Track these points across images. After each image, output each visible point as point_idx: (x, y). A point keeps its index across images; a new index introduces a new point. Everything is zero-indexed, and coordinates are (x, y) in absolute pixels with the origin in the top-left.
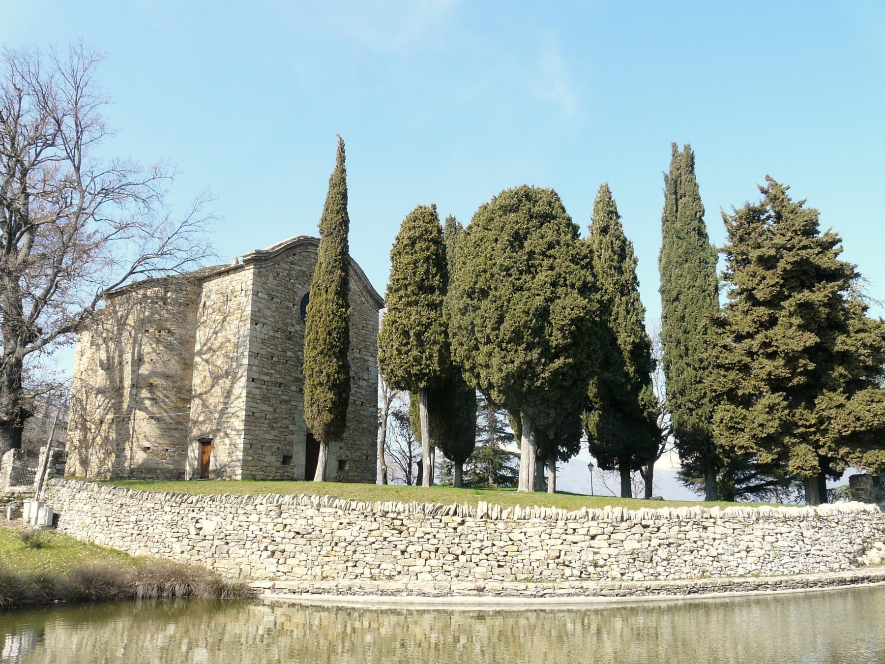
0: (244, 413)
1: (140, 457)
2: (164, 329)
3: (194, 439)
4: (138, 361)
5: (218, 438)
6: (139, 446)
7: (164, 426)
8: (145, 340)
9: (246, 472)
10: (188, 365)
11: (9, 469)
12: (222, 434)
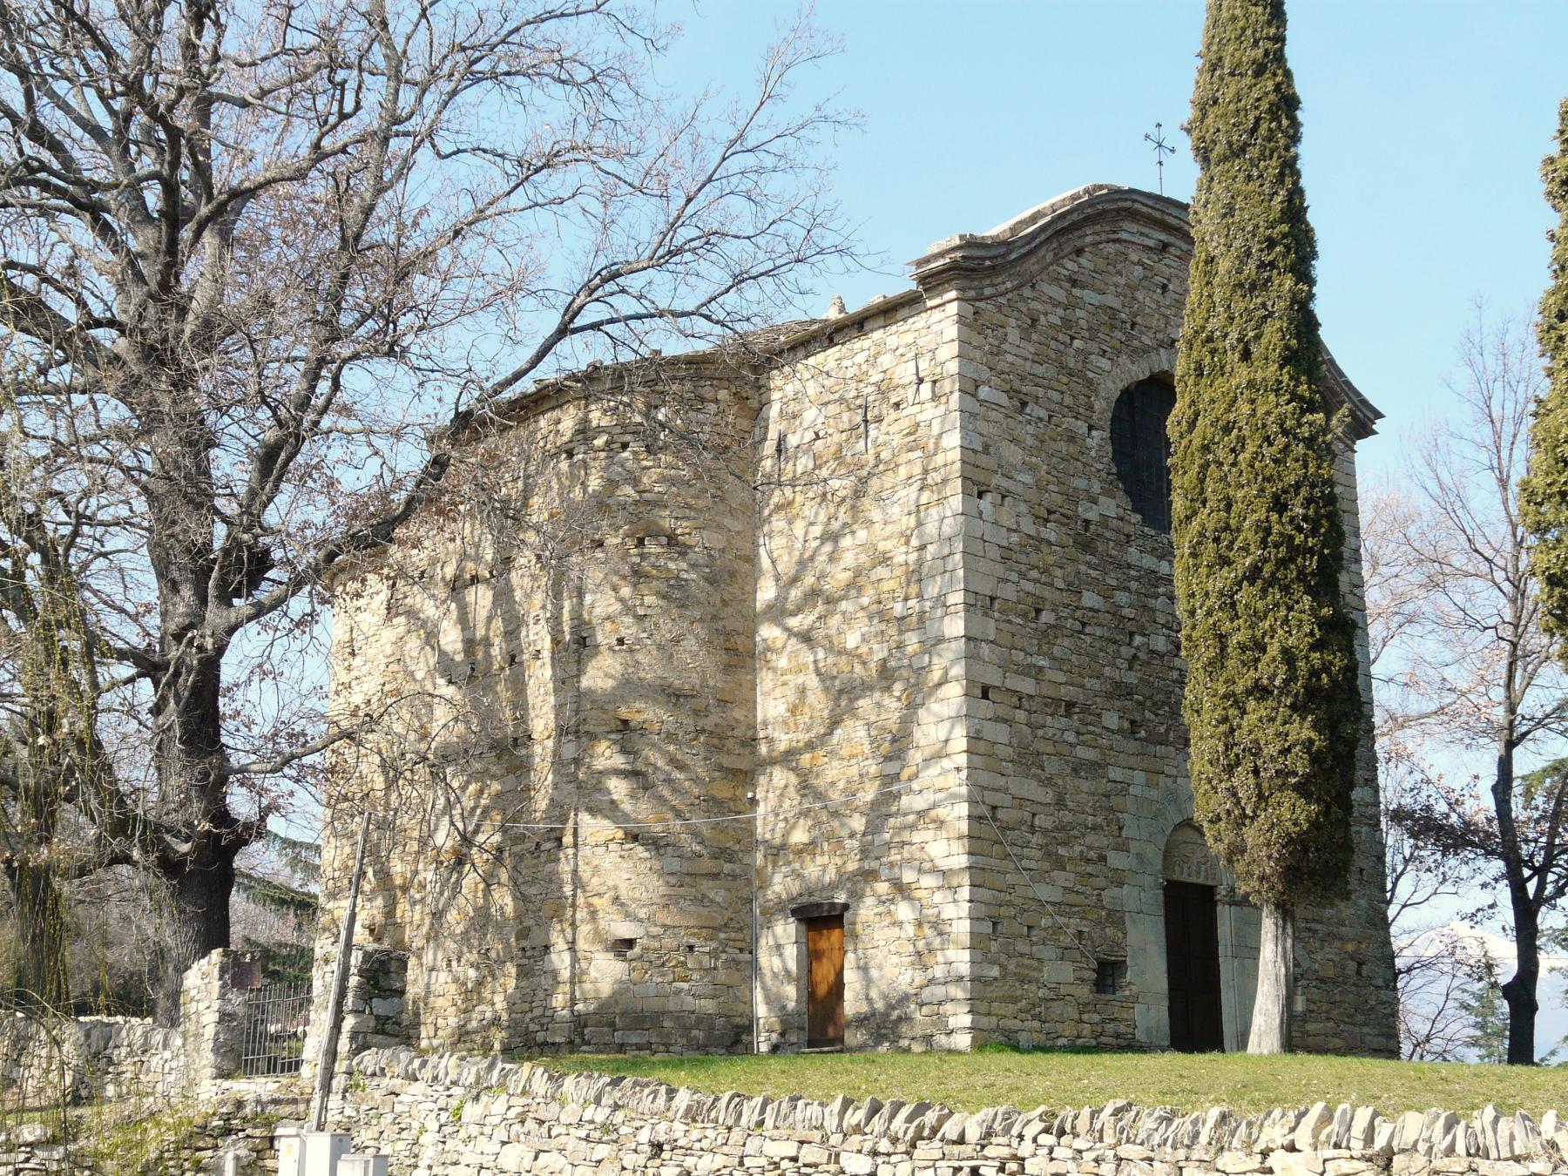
0: (963, 809)
1: (605, 973)
2: (655, 535)
3: (780, 908)
4: (577, 646)
5: (870, 901)
6: (598, 936)
7: (675, 865)
8: (595, 575)
9: (985, 1022)
10: (739, 656)
11: (210, 1018)
12: (883, 887)
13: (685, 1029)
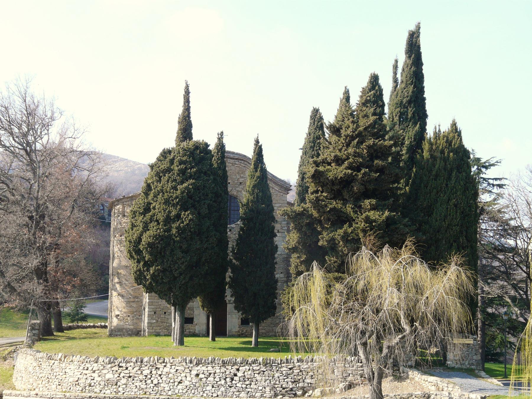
1: (115, 322)
13: (127, 332)
